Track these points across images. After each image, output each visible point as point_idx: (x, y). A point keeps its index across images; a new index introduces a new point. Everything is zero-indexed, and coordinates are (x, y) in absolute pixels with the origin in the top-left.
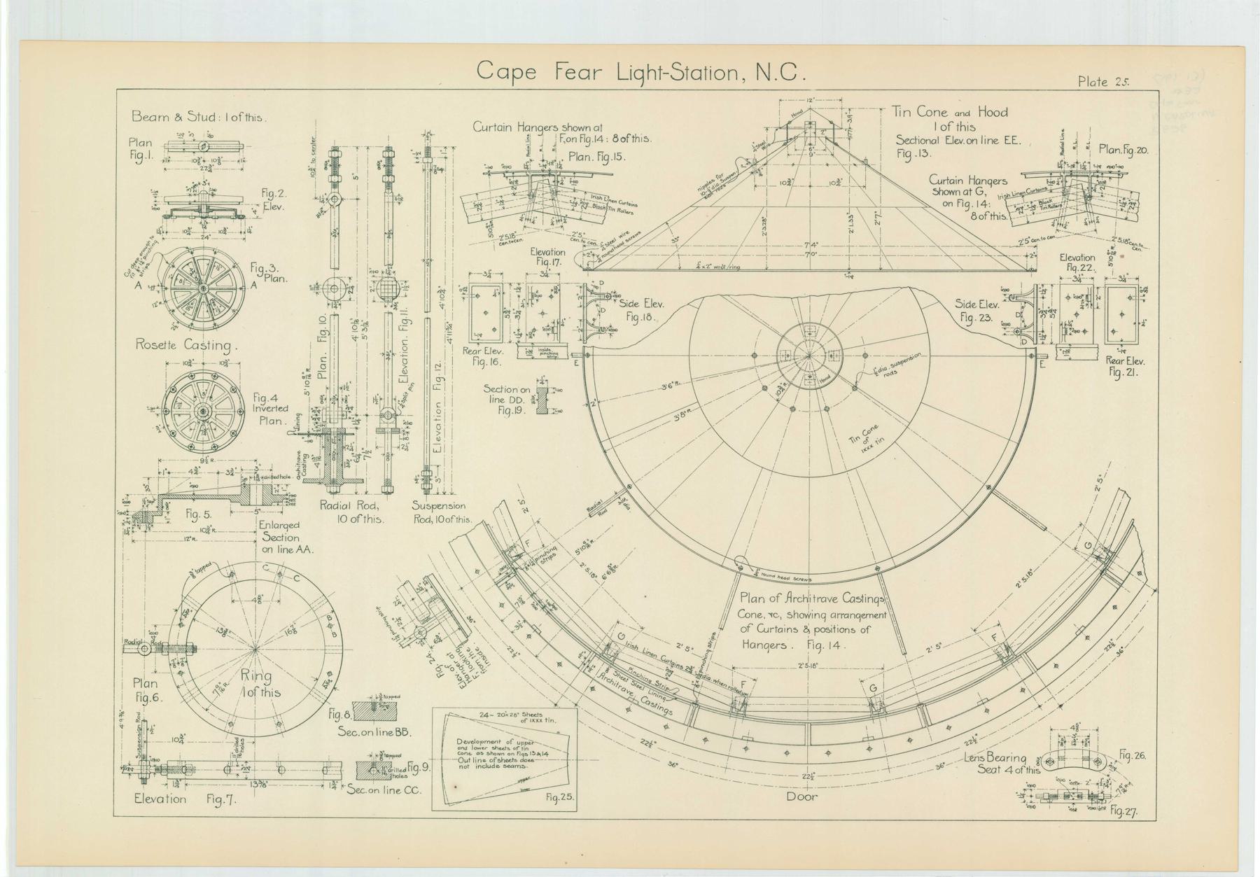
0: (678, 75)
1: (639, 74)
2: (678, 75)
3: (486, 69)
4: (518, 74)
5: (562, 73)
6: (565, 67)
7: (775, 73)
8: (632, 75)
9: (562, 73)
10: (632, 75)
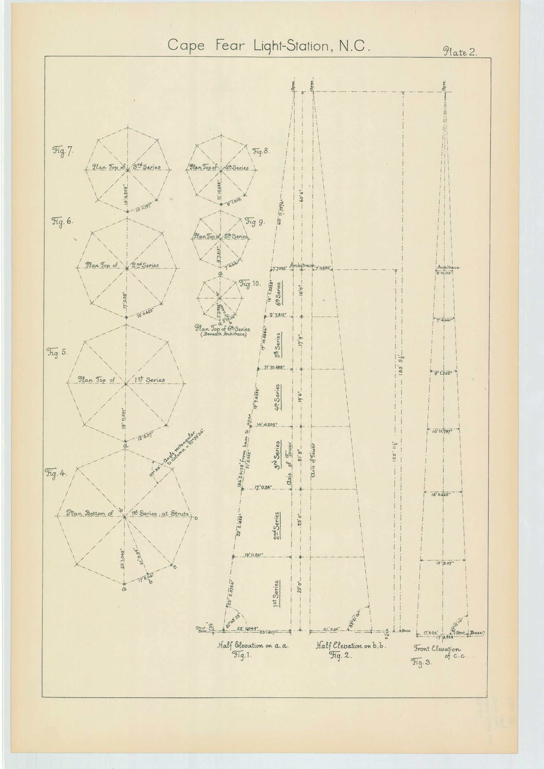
0: (292, 47)
1: (267, 47)
2: (292, 47)
4: (193, 46)
5: (220, 46)
6: (222, 42)
9: (220, 46)
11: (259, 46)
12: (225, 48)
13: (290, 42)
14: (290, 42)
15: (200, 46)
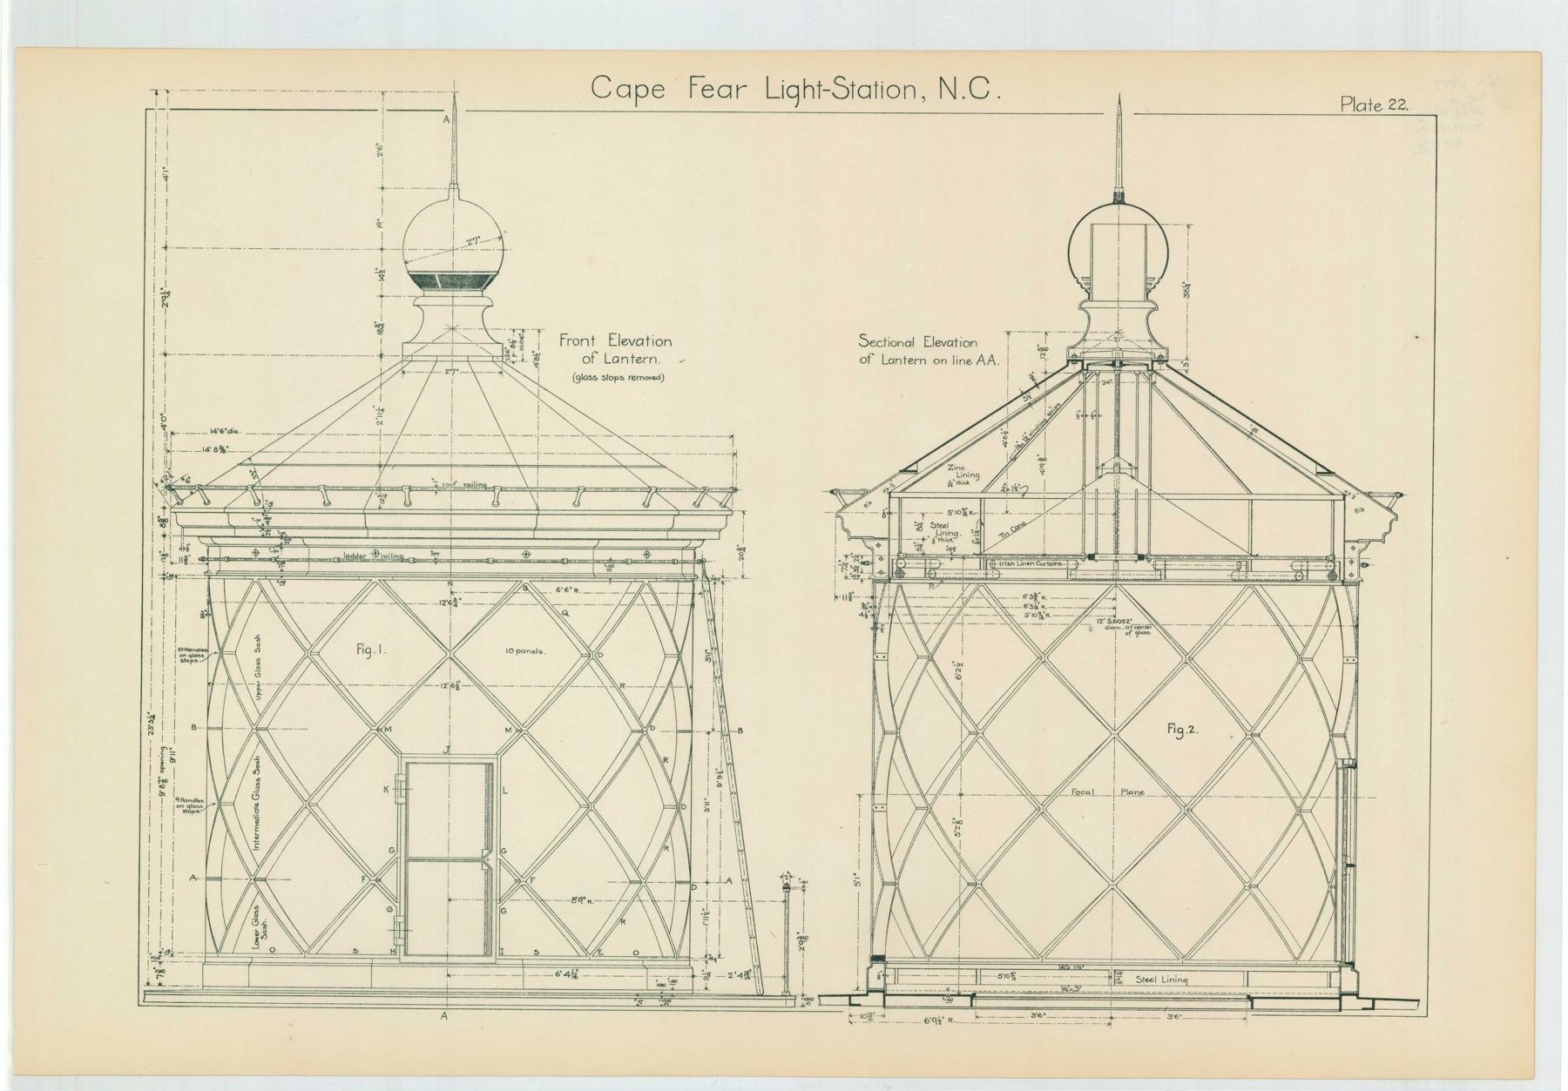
1: (793, 92)
2: (842, 92)
4: (642, 91)
5: (697, 90)
6: (700, 83)
7: (962, 90)
8: (785, 92)
9: (697, 90)
11: (775, 90)
13: (839, 81)
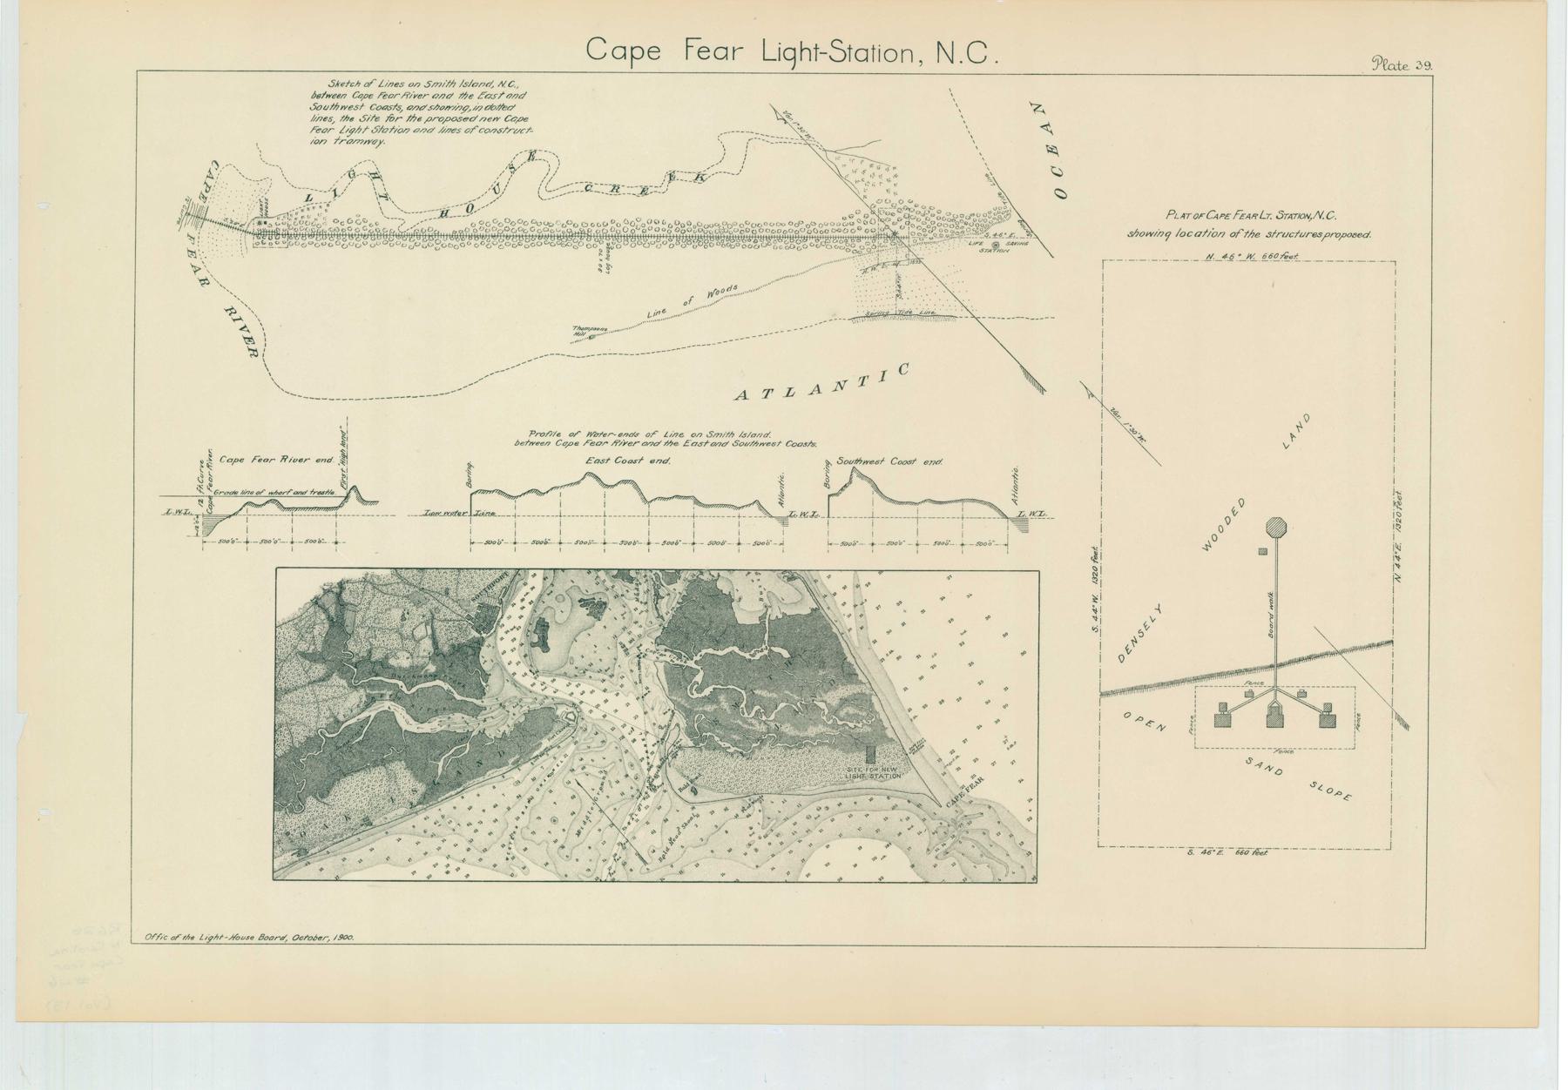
1: (790, 54)
3: (598, 49)
4: (637, 53)
5: (693, 52)
7: (960, 54)
8: (781, 55)
9: (693, 52)
10: (781, 55)
12: (703, 55)
13: (836, 44)
14: (836, 44)
15: (652, 52)
